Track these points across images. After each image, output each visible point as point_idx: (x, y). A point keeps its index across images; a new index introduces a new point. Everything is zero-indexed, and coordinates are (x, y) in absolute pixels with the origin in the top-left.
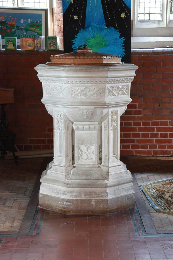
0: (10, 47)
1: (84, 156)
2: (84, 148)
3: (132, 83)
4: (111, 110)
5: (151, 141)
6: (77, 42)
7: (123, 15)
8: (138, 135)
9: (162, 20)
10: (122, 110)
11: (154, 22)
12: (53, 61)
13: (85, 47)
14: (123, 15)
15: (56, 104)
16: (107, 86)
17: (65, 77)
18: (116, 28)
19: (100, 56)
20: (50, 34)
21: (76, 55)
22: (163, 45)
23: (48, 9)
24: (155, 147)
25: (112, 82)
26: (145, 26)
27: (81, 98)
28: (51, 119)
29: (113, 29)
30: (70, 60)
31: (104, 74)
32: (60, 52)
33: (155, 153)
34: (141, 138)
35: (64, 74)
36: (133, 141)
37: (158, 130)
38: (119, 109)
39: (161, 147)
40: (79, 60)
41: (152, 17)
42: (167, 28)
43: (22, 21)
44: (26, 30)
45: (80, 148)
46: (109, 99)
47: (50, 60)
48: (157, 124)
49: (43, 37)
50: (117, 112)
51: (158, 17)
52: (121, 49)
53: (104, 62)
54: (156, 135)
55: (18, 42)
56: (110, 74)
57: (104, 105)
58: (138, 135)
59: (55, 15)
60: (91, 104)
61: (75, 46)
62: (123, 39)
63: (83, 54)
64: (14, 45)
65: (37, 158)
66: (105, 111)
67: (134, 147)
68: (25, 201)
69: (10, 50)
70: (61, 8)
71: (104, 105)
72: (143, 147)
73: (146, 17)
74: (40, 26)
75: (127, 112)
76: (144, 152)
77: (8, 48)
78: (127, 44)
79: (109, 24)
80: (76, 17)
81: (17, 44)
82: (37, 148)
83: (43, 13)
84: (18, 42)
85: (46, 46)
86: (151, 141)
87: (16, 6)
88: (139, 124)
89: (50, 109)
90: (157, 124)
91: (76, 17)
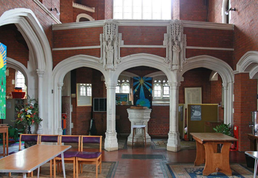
0: (119, 104)
1: (139, 132)
2: (139, 130)
3: (150, 114)
4: (145, 120)
5: (158, 131)
6: (137, 103)
7: (150, 96)
8: (154, 129)
9: (161, 97)
10: (148, 120)
11: (159, 97)
12: (131, 108)
13: (139, 105)
14: (150, 96)
15: (132, 118)
16: (144, 114)
17: (134, 112)
18: (148, 99)
19: (143, 107)
20: (130, 100)
21: (137, 106)
22: (161, 104)
23: (100, 48)
24: (159, 133)
25: (145, 113)
26: (156, 98)
27: (138, 117)
28: (130, 122)
29: (147, 99)
30: (135, 108)
31: (144, 111)
32: (132, 105)
33: (159, 134)
34: (155, 130)
35: (134, 111)
36: (153, 131)
37: (160, 128)
38: (147, 120)
39: (161, 133)
40: (137, 108)
41: (158, 96)
42: (162, 99)
43: (122, 97)
44: (123, 99)
45: (137, 130)
46: (145, 117)
47: (130, 108)
48: (159, 126)
49: (128, 101)
50: (147, 121)
51: (160, 96)
52: (149, 105)
53: (144, 108)
54: (159, 129)
55: (121, 102)
56: (145, 111)
57: (143, 119)
58: (154, 129)
59: (131, 95)
60: (140, 118)
61: (136, 104)
62: (150, 102)
63: (138, 106)
64: (120, 103)
65: (126, 135)
66: (144, 120)
67: (153, 133)
68: (124, 144)
69: (119, 105)
70: (133, 93)
71: (143, 119)
72: (156, 133)
73: (157, 96)
74: (127, 98)
75: (149, 121)
76: (156, 134)
77: (118, 104)
78: (151, 103)
79: (146, 98)
80: (137, 96)
81: (121, 103)
82: (125, 133)
83: (128, 95)
84: (121, 102)
85: (129, 103)
86: (158, 131)
87: (120, 93)
88: (154, 126)
89: (130, 120)
90: (159, 126)
91: (137, 96)
